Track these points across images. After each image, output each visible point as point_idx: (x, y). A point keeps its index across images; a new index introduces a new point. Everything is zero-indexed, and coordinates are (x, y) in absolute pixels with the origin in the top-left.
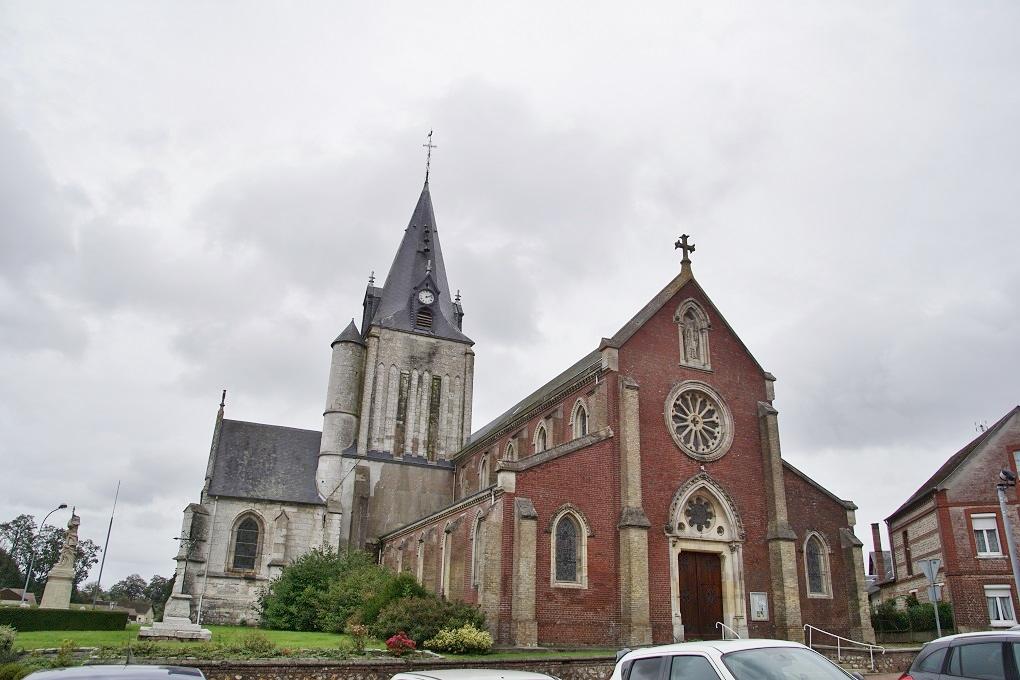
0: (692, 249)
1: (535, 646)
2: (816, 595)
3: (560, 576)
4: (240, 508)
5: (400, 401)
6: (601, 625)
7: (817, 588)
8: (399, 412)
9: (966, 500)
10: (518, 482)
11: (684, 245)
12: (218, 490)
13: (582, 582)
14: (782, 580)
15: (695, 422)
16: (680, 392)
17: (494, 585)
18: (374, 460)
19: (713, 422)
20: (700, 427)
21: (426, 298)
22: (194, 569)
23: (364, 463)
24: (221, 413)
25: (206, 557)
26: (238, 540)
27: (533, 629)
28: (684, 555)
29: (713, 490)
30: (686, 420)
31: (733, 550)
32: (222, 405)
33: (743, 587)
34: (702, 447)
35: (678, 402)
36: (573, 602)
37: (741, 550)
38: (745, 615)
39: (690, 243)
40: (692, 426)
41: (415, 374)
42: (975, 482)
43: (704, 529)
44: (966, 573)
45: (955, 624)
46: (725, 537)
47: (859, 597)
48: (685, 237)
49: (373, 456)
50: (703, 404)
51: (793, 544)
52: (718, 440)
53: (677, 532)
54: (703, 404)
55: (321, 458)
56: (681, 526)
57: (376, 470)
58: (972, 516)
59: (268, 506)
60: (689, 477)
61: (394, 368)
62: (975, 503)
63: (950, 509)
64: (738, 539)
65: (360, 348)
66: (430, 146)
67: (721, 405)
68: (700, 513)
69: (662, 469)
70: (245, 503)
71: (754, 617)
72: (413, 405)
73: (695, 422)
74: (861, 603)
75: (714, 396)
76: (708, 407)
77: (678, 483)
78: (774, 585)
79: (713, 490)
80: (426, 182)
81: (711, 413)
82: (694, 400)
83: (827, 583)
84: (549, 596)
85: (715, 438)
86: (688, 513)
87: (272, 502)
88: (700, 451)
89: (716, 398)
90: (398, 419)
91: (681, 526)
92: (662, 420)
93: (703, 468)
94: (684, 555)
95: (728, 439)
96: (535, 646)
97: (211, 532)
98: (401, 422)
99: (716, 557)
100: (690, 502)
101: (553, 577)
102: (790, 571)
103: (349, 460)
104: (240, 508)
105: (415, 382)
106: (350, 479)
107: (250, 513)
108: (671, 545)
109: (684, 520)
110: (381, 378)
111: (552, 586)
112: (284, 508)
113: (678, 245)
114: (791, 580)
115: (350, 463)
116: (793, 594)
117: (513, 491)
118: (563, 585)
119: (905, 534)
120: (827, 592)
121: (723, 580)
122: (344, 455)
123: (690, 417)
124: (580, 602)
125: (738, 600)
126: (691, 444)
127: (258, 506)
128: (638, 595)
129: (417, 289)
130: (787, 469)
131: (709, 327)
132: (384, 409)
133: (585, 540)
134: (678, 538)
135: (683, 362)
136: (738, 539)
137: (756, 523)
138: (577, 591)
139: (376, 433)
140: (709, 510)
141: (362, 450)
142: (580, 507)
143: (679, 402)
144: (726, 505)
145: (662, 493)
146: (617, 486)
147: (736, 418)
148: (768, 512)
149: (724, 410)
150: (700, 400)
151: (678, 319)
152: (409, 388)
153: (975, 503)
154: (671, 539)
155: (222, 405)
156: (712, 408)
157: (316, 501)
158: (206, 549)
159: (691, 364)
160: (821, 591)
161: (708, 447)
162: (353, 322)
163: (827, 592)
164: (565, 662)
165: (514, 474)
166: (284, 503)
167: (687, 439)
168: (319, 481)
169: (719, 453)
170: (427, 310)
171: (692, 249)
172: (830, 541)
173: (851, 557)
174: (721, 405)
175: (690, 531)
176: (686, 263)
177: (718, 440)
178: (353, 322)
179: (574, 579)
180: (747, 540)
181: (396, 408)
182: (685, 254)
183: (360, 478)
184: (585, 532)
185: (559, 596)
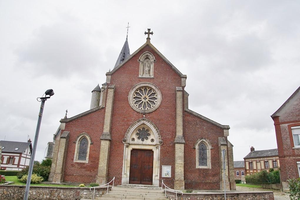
0: (152, 33)
1: (59, 183)
6: (92, 176)
9: (289, 120)
10: (66, 126)
15: (145, 98)
20: (143, 100)
27: (59, 177)
28: (133, 151)
29: (148, 124)
36: (81, 168)
37: (160, 148)
38: (159, 175)
39: (151, 32)
42: (294, 111)
44: (287, 156)
45: (281, 181)
46: (154, 143)
48: (149, 30)
51: (183, 145)
53: (131, 142)
56: (133, 139)
58: (292, 128)
62: (293, 122)
63: (281, 125)
64: (158, 143)
65: (98, 92)
67: (157, 90)
68: (143, 134)
69: (124, 118)
71: (164, 176)
75: (153, 87)
79: (148, 124)
80: (127, 39)
93: (144, 116)
96: (59, 183)
99: (151, 151)
101: (75, 159)
102: (180, 157)
108: (125, 147)
109: (134, 136)
111: (197, 168)
114: (180, 160)
117: (64, 129)
118: (201, 167)
123: (143, 96)
124: (84, 168)
128: (102, 166)
131: (155, 61)
133: (89, 145)
136: (158, 143)
138: (84, 164)
142: (88, 134)
150: (143, 90)
151: (139, 60)
153: (293, 122)
154: (125, 144)
155: (66, 114)
162: (98, 85)
164: (21, 187)
165: (65, 123)
171: (152, 33)
172: (211, 144)
174: (157, 90)
175: (137, 141)
176: (148, 39)
178: (98, 85)
179: (207, 165)
182: (149, 36)
184: (90, 142)
185: (76, 165)
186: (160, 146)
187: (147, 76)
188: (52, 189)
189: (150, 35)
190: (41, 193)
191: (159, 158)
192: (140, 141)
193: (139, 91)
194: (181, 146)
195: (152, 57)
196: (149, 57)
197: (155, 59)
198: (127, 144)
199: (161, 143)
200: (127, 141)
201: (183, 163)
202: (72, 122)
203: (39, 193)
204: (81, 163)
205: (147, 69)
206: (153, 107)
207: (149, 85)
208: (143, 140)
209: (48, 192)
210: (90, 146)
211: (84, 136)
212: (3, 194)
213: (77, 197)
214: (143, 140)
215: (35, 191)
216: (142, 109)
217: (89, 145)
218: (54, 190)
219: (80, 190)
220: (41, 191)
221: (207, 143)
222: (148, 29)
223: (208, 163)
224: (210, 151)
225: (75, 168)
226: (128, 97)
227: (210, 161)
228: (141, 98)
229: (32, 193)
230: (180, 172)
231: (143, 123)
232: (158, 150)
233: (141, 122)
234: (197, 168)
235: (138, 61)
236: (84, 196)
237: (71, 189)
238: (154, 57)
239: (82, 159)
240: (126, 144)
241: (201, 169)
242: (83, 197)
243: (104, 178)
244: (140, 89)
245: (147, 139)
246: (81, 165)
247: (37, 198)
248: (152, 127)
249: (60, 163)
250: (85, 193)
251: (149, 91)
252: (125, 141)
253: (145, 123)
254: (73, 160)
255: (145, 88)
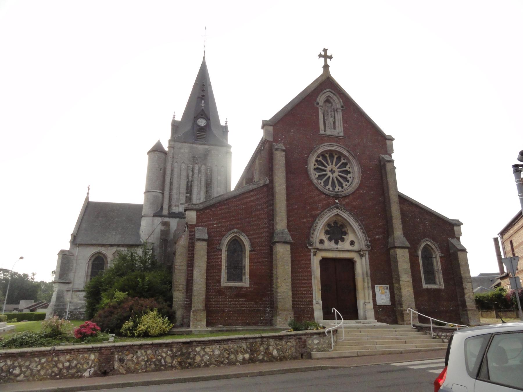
0: (331, 57)
2: (430, 286)
3: (428, 282)
4: (94, 250)
5: (188, 182)
6: (258, 311)
7: (431, 279)
8: (187, 189)
10: (198, 217)
11: (325, 56)
12: (79, 241)
13: (246, 283)
14: (398, 276)
15: (332, 171)
16: (320, 151)
17: (181, 286)
18: (173, 217)
19: (347, 171)
20: (336, 174)
21: (202, 123)
22: (65, 287)
23: (166, 219)
24: (87, 198)
25: (72, 279)
26: (92, 268)
28: (324, 262)
29: (345, 215)
30: (325, 171)
31: (361, 256)
32: (88, 194)
33: (370, 281)
34: (337, 187)
35: (319, 159)
37: (367, 256)
39: (329, 54)
40: (330, 174)
41: (197, 167)
43: (340, 242)
46: (356, 247)
47: (464, 287)
49: (172, 215)
50: (339, 159)
51: (407, 250)
52: (350, 183)
53: (318, 245)
54: (339, 159)
55: (143, 218)
56: (322, 242)
57: (174, 223)
59: (109, 248)
60: (328, 207)
61: (183, 165)
64: (365, 248)
66: (205, 36)
67: (351, 158)
70: (95, 247)
71: (379, 302)
72: (196, 184)
73: (332, 171)
74: (466, 291)
75: (345, 153)
76: (343, 161)
77: (318, 212)
78: (394, 280)
79: (345, 215)
81: (344, 165)
82: (332, 156)
83: (440, 277)
84: (221, 292)
85: (348, 181)
86: (327, 232)
87: (111, 245)
88: (336, 190)
89: (347, 154)
90: (187, 193)
91: (322, 242)
92: (306, 173)
93: (337, 201)
94: (324, 262)
95: (357, 182)
97: (75, 265)
98: (189, 195)
99: (351, 263)
100: (329, 225)
103: (157, 219)
104: (94, 250)
105: (196, 171)
106: (159, 228)
107: (100, 253)
109: (324, 237)
110: (176, 170)
111: (248, 286)
112: (119, 249)
113: (320, 56)
115: (158, 220)
116: (408, 286)
117: (194, 223)
119: (511, 242)
120: (440, 284)
121: (356, 277)
122: (155, 215)
123: (328, 168)
125: (366, 291)
126: (329, 186)
127: (103, 248)
129: (196, 118)
130: (404, 200)
131: (342, 107)
132: (179, 188)
134: (317, 249)
135: (322, 132)
136: (365, 248)
137: (379, 237)
138: (242, 288)
139: (174, 202)
140: (343, 230)
141: (165, 212)
143: (320, 159)
144: (355, 225)
145: (305, 220)
146: (271, 216)
147: (362, 166)
148: (388, 231)
149: (354, 162)
150: (336, 157)
152: (193, 175)
154: (312, 251)
156: (345, 161)
157: (138, 243)
158: (71, 276)
159: (329, 132)
160: (435, 283)
161: (342, 187)
163: (440, 284)
166: (119, 246)
167: (326, 183)
168: (141, 232)
169: (351, 190)
170: (202, 129)
171: (331, 57)
172: (441, 248)
173: (456, 259)
174: (351, 158)
175: (329, 244)
176: (326, 67)
177: (350, 183)
180: (372, 249)
181: (185, 187)
182: (326, 61)
183: (163, 228)
184: (248, 248)
186: (367, 253)
187: (335, 133)
188: (251, 340)
189: (328, 60)
190: (232, 350)
191: (89, 274)
192: (332, 245)
193: (321, 157)
194: (404, 252)
195: (337, 100)
196: (331, 100)
197: (342, 104)
198: (315, 250)
199: (369, 247)
200: (314, 245)
201: (410, 280)
202: (208, 209)
203: (227, 350)
204: (236, 287)
205: (331, 120)
206: (347, 187)
207: (339, 149)
208: (337, 243)
209: (244, 346)
210: (249, 255)
211: (236, 236)
212: (147, 361)
213: (304, 350)
214: (337, 243)
215: (218, 346)
216: (329, 189)
217: (247, 253)
218: (256, 342)
219: (307, 336)
220: (233, 346)
221: (433, 247)
222: (327, 49)
223: (437, 280)
224: (439, 259)
225: (226, 296)
226: (306, 168)
227: (441, 276)
228: (325, 171)
229: (211, 353)
230: (408, 296)
231: (336, 213)
232: (364, 259)
233: (333, 212)
234: (248, 286)
235: (315, 105)
236: (315, 347)
237: (289, 337)
238: (341, 101)
239: (234, 280)
240: (314, 250)
241: (431, 289)
242: (313, 350)
243: (290, 313)
244: (323, 155)
245: (343, 240)
246: (239, 293)
247: (223, 361)
248: (351, 220)
249: (200, 289)
250: (316, 342)
251: (337, 158)
252: (311, 244)
253: (340, 214)
254: (219, 281)
255: (331, 153)
